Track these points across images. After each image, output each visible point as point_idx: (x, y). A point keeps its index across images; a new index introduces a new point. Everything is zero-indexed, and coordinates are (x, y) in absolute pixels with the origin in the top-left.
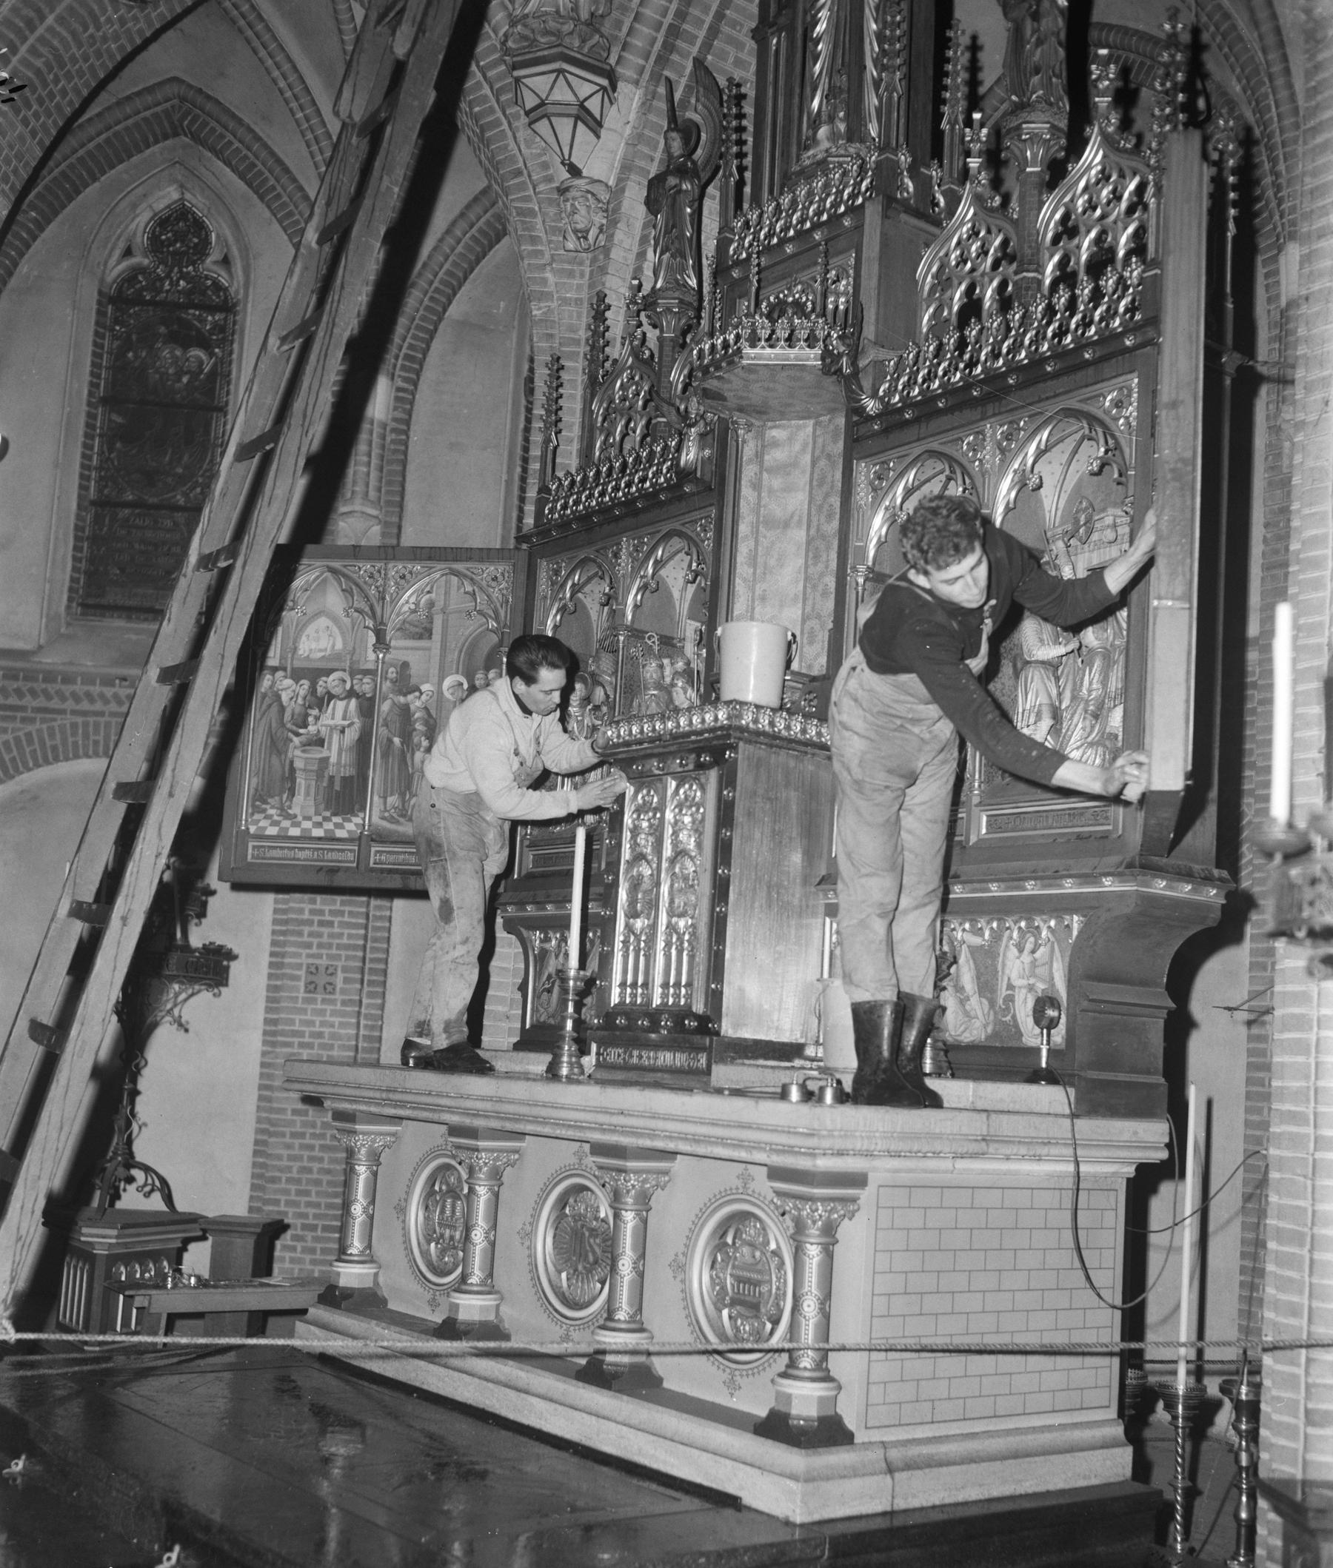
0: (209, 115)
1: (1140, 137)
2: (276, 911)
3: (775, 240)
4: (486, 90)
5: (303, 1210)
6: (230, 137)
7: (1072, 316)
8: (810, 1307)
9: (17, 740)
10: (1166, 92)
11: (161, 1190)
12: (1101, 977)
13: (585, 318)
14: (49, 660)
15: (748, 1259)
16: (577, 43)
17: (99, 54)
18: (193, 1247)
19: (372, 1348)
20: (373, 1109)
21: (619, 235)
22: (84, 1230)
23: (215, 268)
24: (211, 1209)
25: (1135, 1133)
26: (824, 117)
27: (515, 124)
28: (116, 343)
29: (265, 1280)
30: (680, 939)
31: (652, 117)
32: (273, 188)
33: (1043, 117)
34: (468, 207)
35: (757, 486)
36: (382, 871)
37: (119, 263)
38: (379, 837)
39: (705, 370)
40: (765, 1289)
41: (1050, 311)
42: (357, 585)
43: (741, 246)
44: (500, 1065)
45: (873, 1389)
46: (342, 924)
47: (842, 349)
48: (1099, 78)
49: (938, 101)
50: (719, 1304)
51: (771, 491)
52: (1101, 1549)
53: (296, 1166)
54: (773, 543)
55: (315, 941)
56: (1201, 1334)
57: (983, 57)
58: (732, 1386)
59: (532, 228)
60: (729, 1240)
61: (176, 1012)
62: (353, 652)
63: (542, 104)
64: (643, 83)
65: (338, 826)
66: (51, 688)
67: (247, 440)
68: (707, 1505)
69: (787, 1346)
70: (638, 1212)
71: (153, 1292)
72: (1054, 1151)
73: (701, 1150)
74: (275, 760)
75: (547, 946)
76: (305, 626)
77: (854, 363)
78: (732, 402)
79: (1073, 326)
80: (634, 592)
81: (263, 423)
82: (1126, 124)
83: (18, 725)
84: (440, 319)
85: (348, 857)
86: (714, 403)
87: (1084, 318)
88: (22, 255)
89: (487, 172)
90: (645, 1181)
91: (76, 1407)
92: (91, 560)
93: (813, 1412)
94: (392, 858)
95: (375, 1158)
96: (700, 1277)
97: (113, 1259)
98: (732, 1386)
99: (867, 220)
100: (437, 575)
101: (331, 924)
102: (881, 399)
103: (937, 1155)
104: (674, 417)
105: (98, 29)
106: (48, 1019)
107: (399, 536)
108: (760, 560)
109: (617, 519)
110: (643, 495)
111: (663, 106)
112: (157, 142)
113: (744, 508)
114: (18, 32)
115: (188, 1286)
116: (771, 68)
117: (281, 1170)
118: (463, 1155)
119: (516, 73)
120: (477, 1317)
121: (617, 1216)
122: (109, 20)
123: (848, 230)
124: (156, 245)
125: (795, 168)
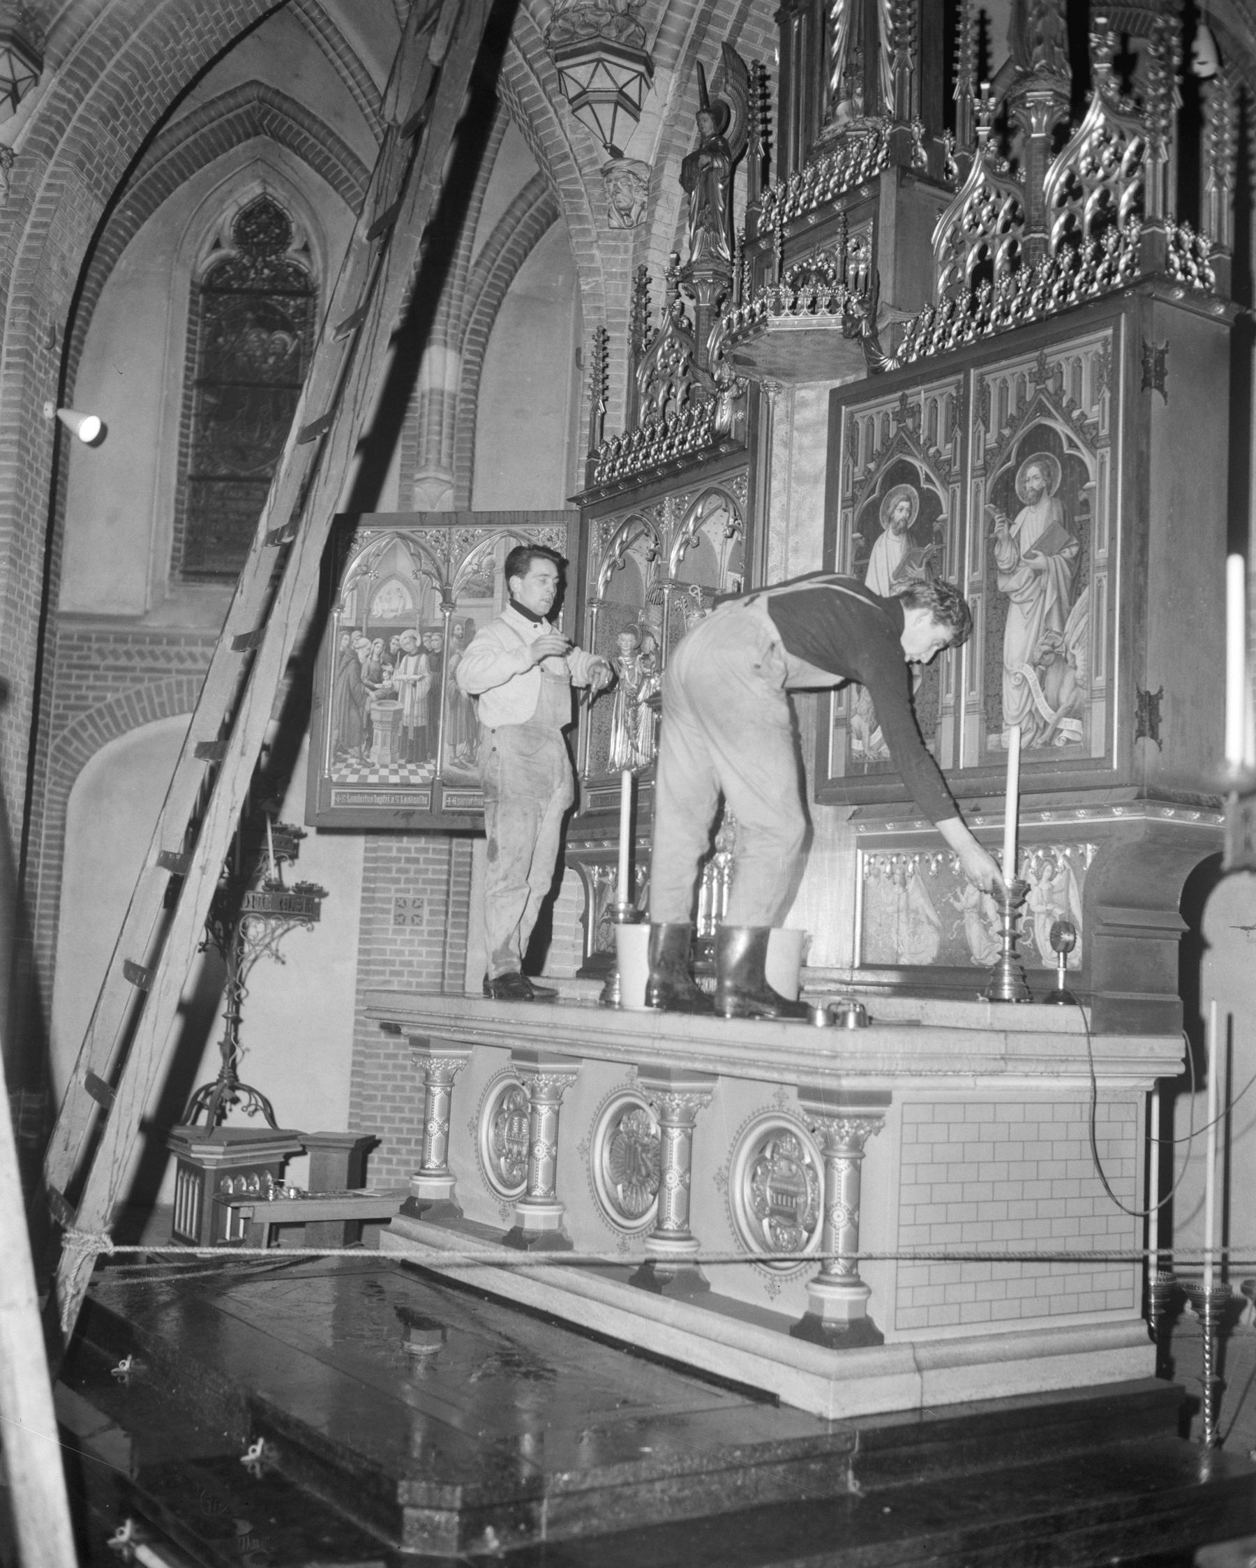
0: (287, 114)
1: (1139, 101)
2: (366, 850)
3: (799, 212)
4: (534, 81)
5: (397, 1125)
6: (306, 134)
7: (1075, 274)
8: (840, 1217)
9: (128, 698)
10: (1161, 57)
11: (264, 1110)
12: (1113, 903)
13: (630, 291)
14: (156, 624)
15: (785, 1172)
16: (614, 33)
17: (179, 66)
18: (294, 1161)
19: (458, 1256)
20: (445, 1035)
21: (659, 212)
22: (194, 1148)
23: (296, 256)
24: (310, 1127)
25: (1152, 1049)
26: (842, 94)
27: (561, 111)
28: (208, 330)
29: (358, 1192)
30: (721, 873)
31: (687, 99)
32: (347, 179)
33: (1044, 84)
34: (526, 188)
35: (788, 444)
36: (453, 813)
37: (209, 254)
38: (450, 782)
39: (734, 339)
40: (801, 1200)
41: (1056, 269)
42: (424, 549)
43: (768, 219)
44: (564, 991)
45: (902, 1293)
46: (427, 861)
47: (861, 313)
48: (1099, 46)
49: (950, 74)
50: (760, 1213)
51: (801, 448)
52: (1125, 1442)
53: (390, 1084)
54: (804, 498)
55: (403, 877)
56: (1225, 1241)
57: (992, 30)
58: (773, 1290)
59: (577, 208)
60: (768, 1154)
61: (273, 945)
62: (422, 612)
63: (584, 92)
64: (679, 66)
65: (413, 772)
66: (158, 649)
67: (308, 424)
68: (748, 1402)
69: (817, 1255)
70: (684, 1130)
71: (256, 1204)
72: (1073, 1067)
73: (737, 1071)
74: (354, 713)
75: (604, 880)
76: (379, 587)
77: (873, 326)
78: (761, 366)
79: (1077, 284)
80: (677, 547)
81: (322, 408)
82: (1125, 89)
83: (128, 684)
84: (503, 295)
85: (421, 801)
86: (745, 368)
87: (1110, 266)
88: (120, 251)
89: (538, 159)
90: (689, 1101)
91: (174, 1313)
92: (190, 531)
93: (844, 1315)
94: (462, 801)
95: (449, 1080)
96: (741, 1189)
97: (221, 1174)
98: (773, 1290)
99: (883, 189)
100: (497, 538)
101: (416, 861)
102: (900, 359)
103: (957, 1073)
104: (709, 383)
105: (178, 43)
106: (142, 961)
107: (470, 499)
108: (793, 514)
109: (660, 480)
110: (685, 457)
111: (695, 87)
112: (240, 141)
113: (776, 464)
114: (105, 49)
115: (288, 1198)
116: (793, 48)
117: (375, 1088)
118: (525, 1077)
119: (560, 64)
120: (542, 1227)
121: (664, 1132)
122: (188, 34)
123: (866, 200)
124: (241, 237)
125: (816, 143)
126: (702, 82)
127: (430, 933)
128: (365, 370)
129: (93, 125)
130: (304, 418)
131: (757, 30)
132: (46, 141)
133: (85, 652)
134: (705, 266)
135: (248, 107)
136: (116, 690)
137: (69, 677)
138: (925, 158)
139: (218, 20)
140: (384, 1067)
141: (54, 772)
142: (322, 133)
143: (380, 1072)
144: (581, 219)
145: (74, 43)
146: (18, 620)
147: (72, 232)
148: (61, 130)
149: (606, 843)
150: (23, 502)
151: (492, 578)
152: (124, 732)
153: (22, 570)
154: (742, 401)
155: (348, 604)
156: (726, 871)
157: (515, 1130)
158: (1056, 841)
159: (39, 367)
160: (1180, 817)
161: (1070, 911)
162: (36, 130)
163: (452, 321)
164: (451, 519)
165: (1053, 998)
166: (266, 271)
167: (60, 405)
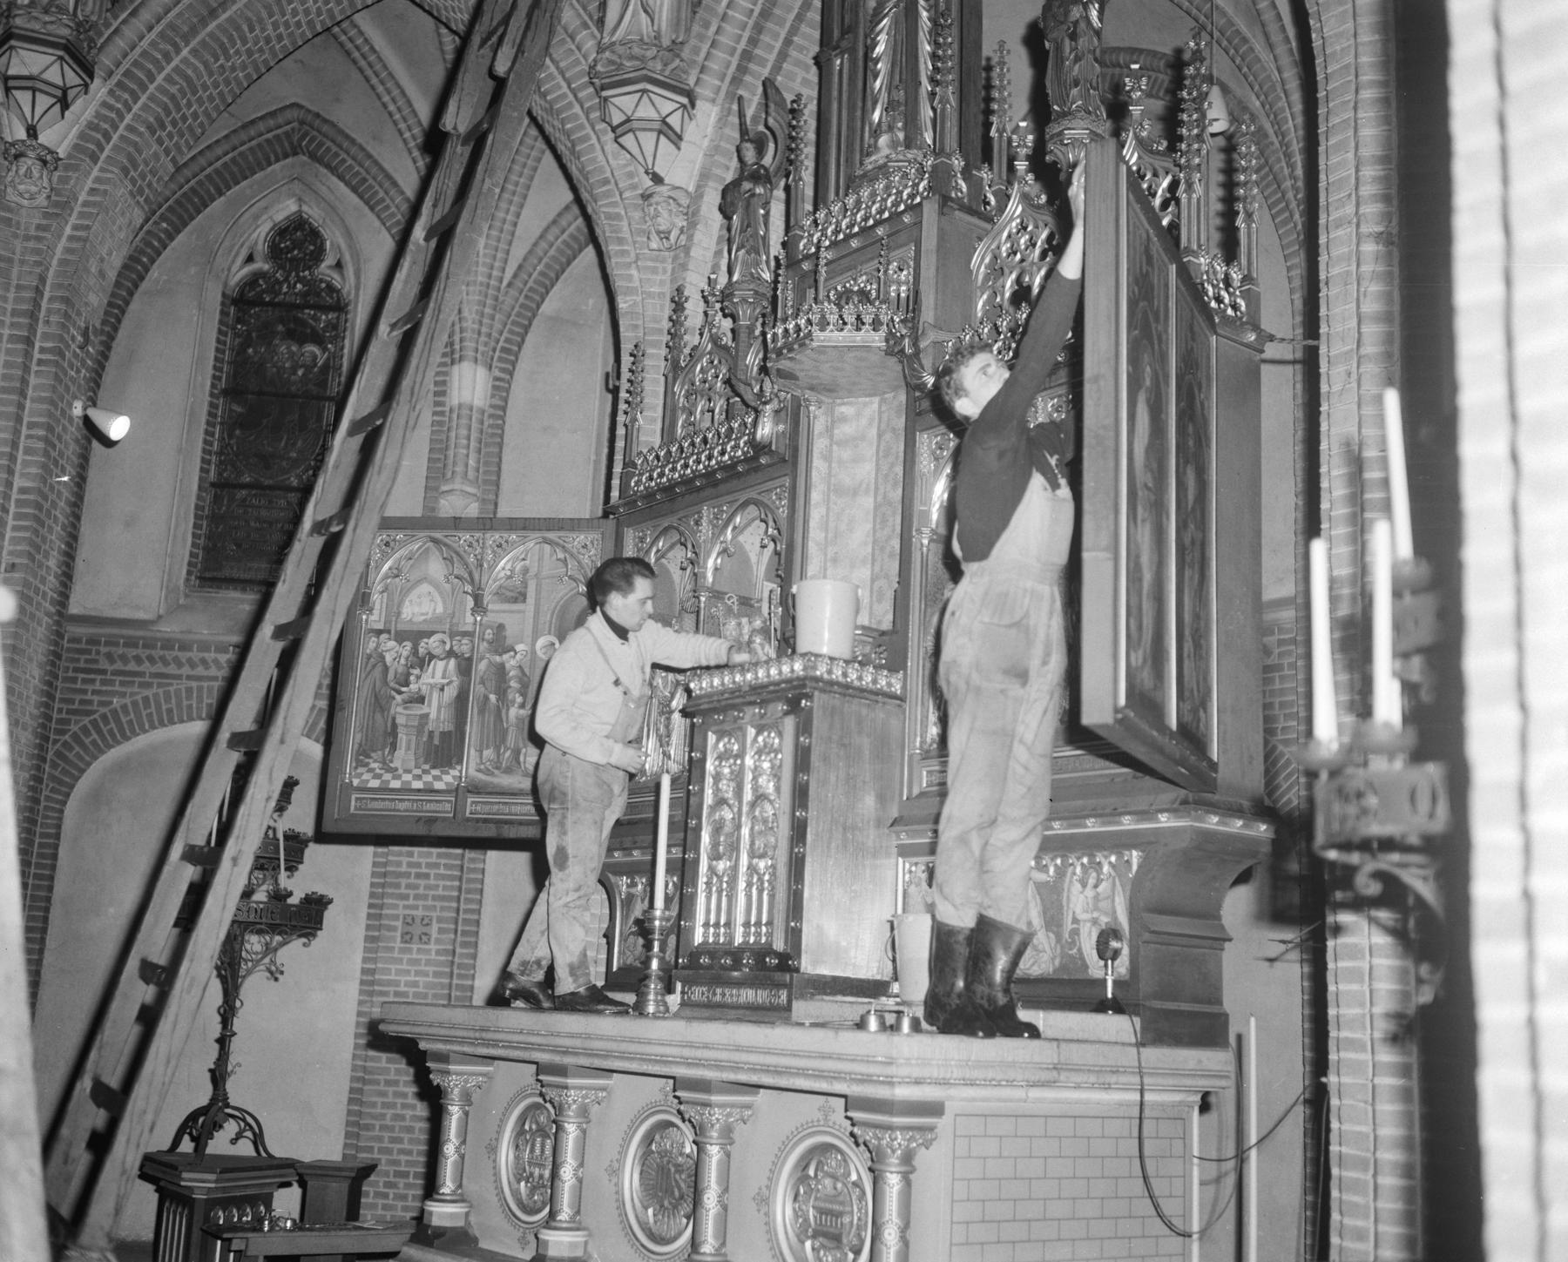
0: (325, 136)
3: (841, 236)
4: (577, 109)
6: (343, 155)
9: (135, 704)
14: (168, 628)
15: (830, 1190)
16: (659, 67)
20: (467, 1049)
21: (698, 236)
22: (185, 1175)
25: (1200, 1061)
26: (884, 127)
27: (603, 139)
30: (760, 880)
31: (727, 131)
32: (383, 200)
35: (827, 458)
36: (478, 820)
37: (241, 268)
38: (475, 789)
40: (846, 1220)
42: (458, 554)
51: (840, 462)
55: (412, 892)
59: (617, 230)
60: (811, 1172)
62: (453, 616)
63: (628, 120)
65: (436, 778)
66: (169, 655)
67: (359, 417)
71: (250, 1235)
72: (1123, 1079)
74: (378, 716)
75: (633, 890)
76: (409, 590)
77: (915, 344)
80: (714, 555)
84: (534, 316)
85: (445, 808)
86: (787, 382)
88: (153, 261)
90: (729, 1115)
92: (209, 537)
94: (487, 808)
96: (783, 1210)
97: (212, 1204)
101: (427, 876)
108: (832, 525)
109: (699, 489)
110: (723, 467)
112: (277, 160)
114: (156, 62)
115: (285, 1229)
119: (604, 94)
122: (237, 52)
123: (907, 227)
124: (275, 252)
125: (859, 172)
126: (741, 115)
127: (438, 952)
128: (422, 366)
129: (140, 134)
130: (355, 411)
131: (796, 70)
132: (93, 147)
133: (93, 656)
134: (745, 286)
135: (288, 128)
136: (123, 695)
137: (74, 680)
138: (965, 189)
139: (268, 40)
140: (384, 1094)
141: (53, 778)
142: (360, 156)
143: (379, 1100)
144: (621, 241)
145: (125, 55)
146: (32, 616)
147: (112, 235)
148: (108, 138)
149: (635, 853)
150: (45, 498)
151: (525, 584)
152: (128, 739)
153: (40, 566)
154: (783, 414)
155: (377, 606)
156: (767, 877)
157: (538, 1152)
158: (1101, 848)
159: (71, 366)
160: (1225, 824)
161: (1115, 919)
162: (82, 136)
163: (483, 339)
164: (487, 523)
165: (1101, 1006)
166: (299, 286)
167: (93, 402)
